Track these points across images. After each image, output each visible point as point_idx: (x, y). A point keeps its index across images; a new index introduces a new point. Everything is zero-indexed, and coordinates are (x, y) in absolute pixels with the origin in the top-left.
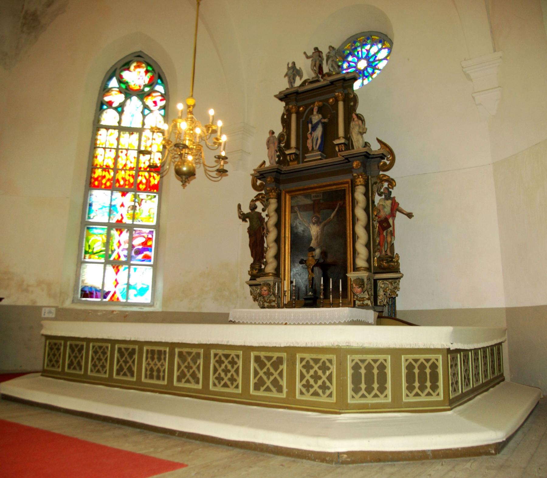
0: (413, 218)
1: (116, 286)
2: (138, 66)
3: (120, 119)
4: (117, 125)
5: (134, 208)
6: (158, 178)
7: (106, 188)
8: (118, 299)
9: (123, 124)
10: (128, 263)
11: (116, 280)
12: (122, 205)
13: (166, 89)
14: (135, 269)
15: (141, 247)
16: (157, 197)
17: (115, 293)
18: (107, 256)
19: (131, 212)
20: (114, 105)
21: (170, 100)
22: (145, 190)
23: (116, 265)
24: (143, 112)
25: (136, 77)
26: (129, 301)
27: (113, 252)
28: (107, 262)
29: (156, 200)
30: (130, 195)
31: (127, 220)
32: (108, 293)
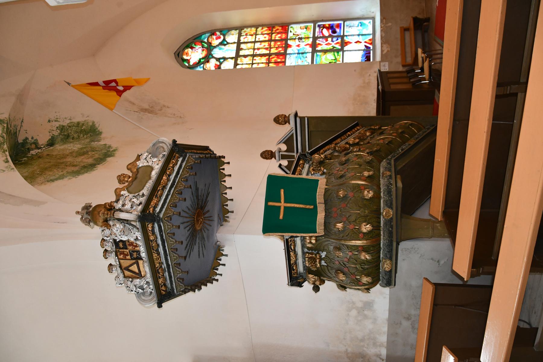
0: (314, 292)
1: (361, 42)
2: (187, 54)
3: (230, 58)
4: (234, 60)
5: (300, 39)
6: (277, 27)
7: (285, 58)
8: (370, 40)
9: (234, 55)
10: (342, 37)
11: (356, 42)
12: (298, 46)
13: (204, 33)
14: (347, 32)
15: (330, 31)
16: (292, 26)
17: (365, 42)
18: (338, 51)
19: (303, 40)
20: (218, 63)
21: (214, 28)
22: (287, 33)
23: (344, 44)
24: (225, 45)
25: (195, 55)
26: (371, 33)
27: (334, 47)
28: (342, 50)
29: (294, 26)
30: (290, 42)
31: (310, 41)
32: (365, 46)
